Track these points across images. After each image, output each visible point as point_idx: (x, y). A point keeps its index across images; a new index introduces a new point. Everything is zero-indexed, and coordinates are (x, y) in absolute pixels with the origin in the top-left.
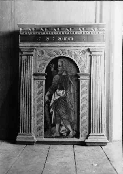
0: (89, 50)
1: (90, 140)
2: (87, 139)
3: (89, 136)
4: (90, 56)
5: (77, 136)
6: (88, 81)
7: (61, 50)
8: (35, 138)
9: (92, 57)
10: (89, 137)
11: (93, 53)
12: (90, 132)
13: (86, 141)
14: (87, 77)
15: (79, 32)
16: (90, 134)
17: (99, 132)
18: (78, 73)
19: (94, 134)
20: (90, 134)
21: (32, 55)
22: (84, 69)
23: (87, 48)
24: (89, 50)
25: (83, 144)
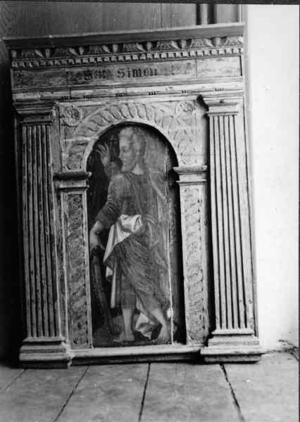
1: (211, 350)
2: (206, 344)
3: (211, 336)
4: (206, 117)
5: (181, 337)
8: (66, 346)
10: (210, 341)
11: (212, 109)
12: (213, 327)
13: (205, 351)
15: (107, 57)
16: (213, 333)
17: (239, 326)
18: (175, 168)
19: (224, 331)
20: (213, 333)
22: (190, 157)
23: (195, 97)
24: (200, 100)
25: (195, 359)
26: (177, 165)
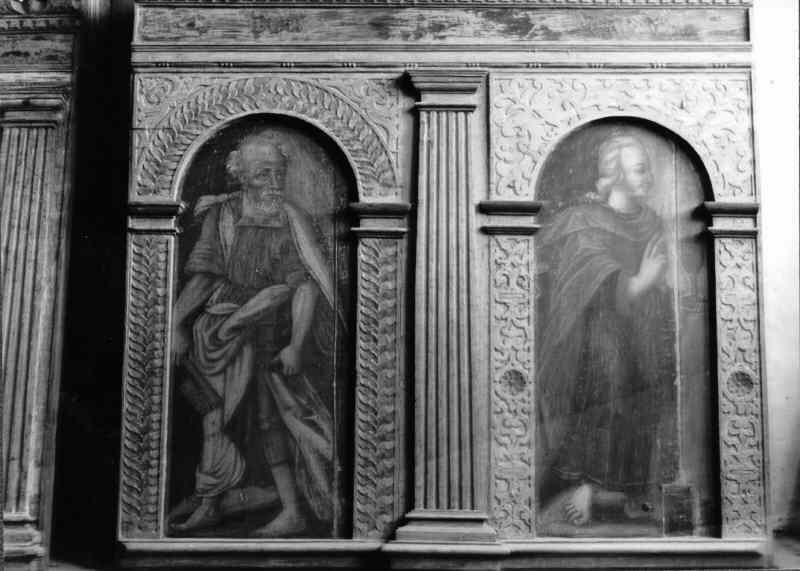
0: (405, 85)
3: (404, 521)
4: (415, 113)
6: (403, 243)
7: (405, 85)
9: (424, 116)
12: (410, 504)
13: (391, 547)
26: (357, 199)
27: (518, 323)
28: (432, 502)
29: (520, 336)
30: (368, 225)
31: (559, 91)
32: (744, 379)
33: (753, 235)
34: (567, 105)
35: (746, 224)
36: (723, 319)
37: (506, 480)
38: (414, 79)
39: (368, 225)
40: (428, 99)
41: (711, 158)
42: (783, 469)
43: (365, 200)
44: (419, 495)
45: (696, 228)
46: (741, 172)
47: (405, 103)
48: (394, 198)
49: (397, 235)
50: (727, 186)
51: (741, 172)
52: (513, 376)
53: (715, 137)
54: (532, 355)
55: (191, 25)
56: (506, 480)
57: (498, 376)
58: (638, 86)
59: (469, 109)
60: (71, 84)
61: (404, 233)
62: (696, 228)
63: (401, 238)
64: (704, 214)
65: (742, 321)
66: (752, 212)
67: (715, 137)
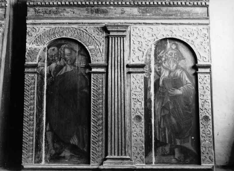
3: (105, 159)
4: (107, 38)
6: (104, 76)
7: (105, 29)
12: (106, 154)
13: (101, 167)
14: (103, 70)
16: (106, 157)
20: (106, 157)
21: (124, 36)
26: (90, 62)
27: (140, 100)
28: (116, 154)
29: (140, 105)
30: (94, 70)
31: (152, 31)
32: (206, 118)
33: (210, 73)
34: (154, 35)
35: (208, 70)
36: (200, 99)
37: (136, 147)
38: (107, 28)
39: (94, 70)
40: (111, 34)
41: (197, 51)
42: (227, 147)
43: (93, 62)
44: (109, 151)
45: (193, 71)
46: (134, 44)
47: (105, 34)
48: (103, 62)
49: (102, 73)
50: (202, 57)
51: (134, 44)
52: (138, 117)
53: (141, 37)
54: (143, 111)
55: (80, 15)
56: (136, 147)
57: (133, 117)
58: (179, 29)
59: (124, 36)
60: (64, 40)
61: (105, 72)
62: (193, 71)
63: (105, 73)
64: (195, 67)
65: (206, 100)
66: (209, 67)
67: (141, 37)
